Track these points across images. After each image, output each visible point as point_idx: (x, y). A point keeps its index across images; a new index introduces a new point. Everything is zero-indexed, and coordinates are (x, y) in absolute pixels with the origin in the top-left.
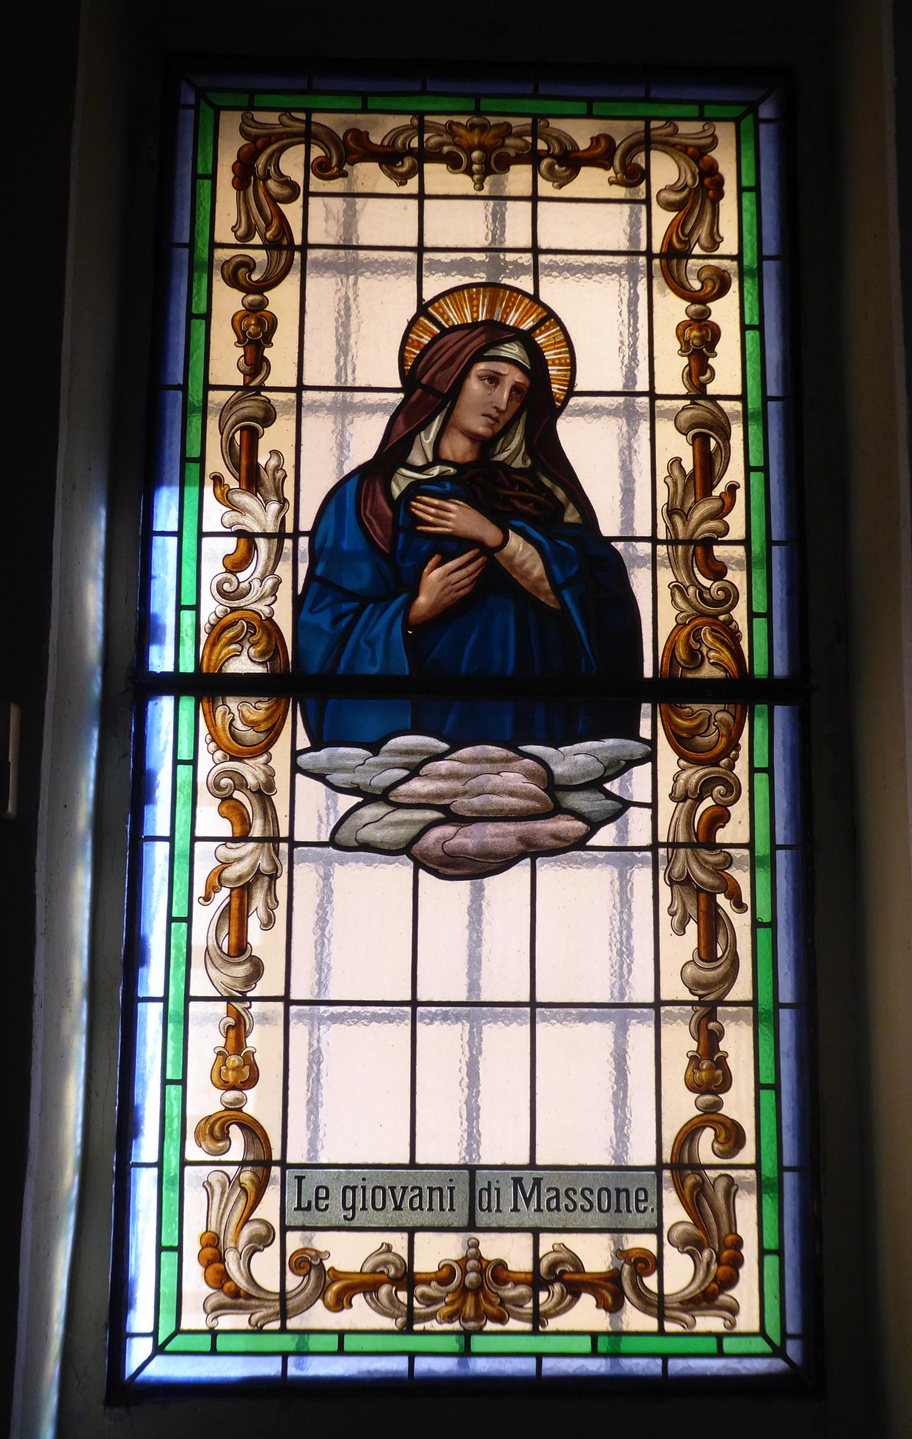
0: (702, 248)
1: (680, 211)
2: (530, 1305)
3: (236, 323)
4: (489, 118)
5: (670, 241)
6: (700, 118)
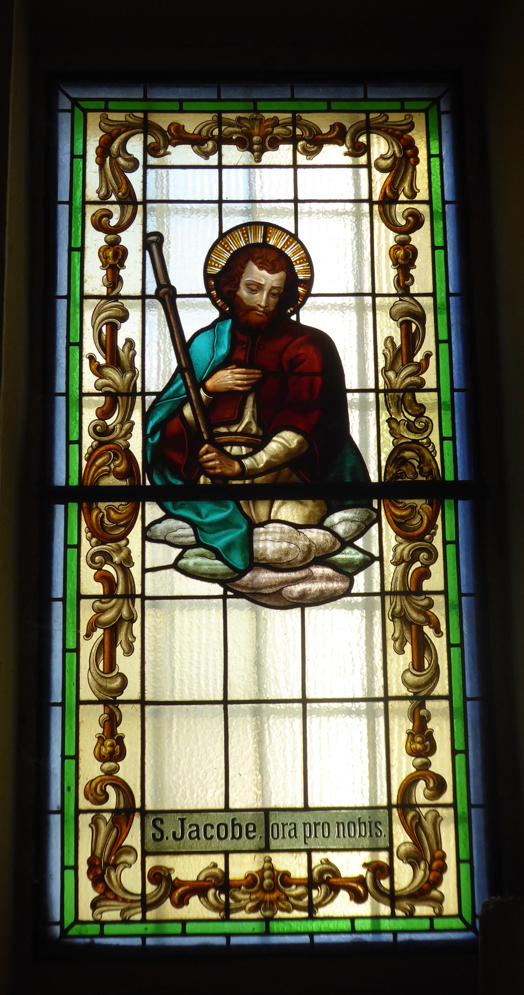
0: (406, 195)
1: (390, 171)
2: (306, 899)
3: (102, 254)
4: (264, 114)
5: (385, 192)
6: (402, 110)
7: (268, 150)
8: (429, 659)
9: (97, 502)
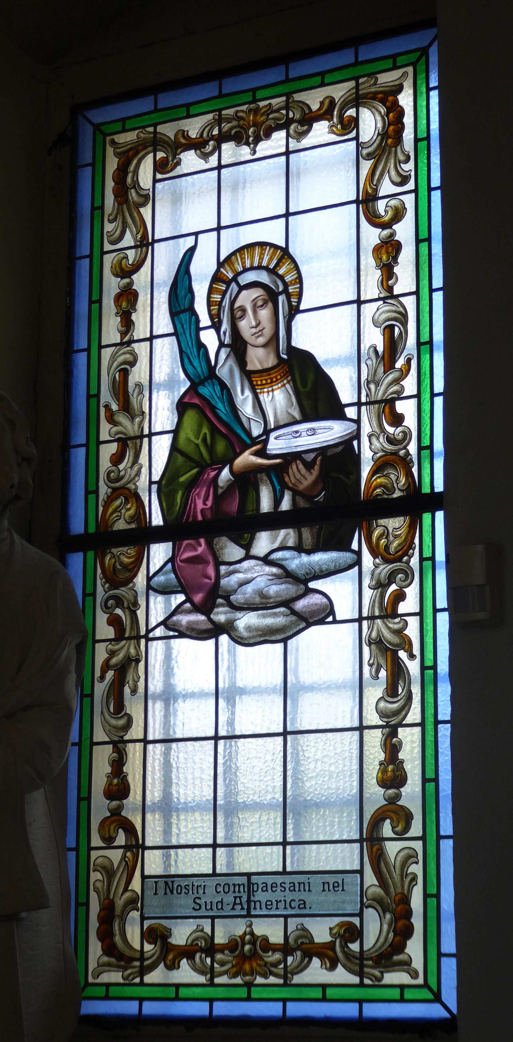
2: (282, 966)
7: (263, 140)
8: (402, 684)
9: (110, 549)
